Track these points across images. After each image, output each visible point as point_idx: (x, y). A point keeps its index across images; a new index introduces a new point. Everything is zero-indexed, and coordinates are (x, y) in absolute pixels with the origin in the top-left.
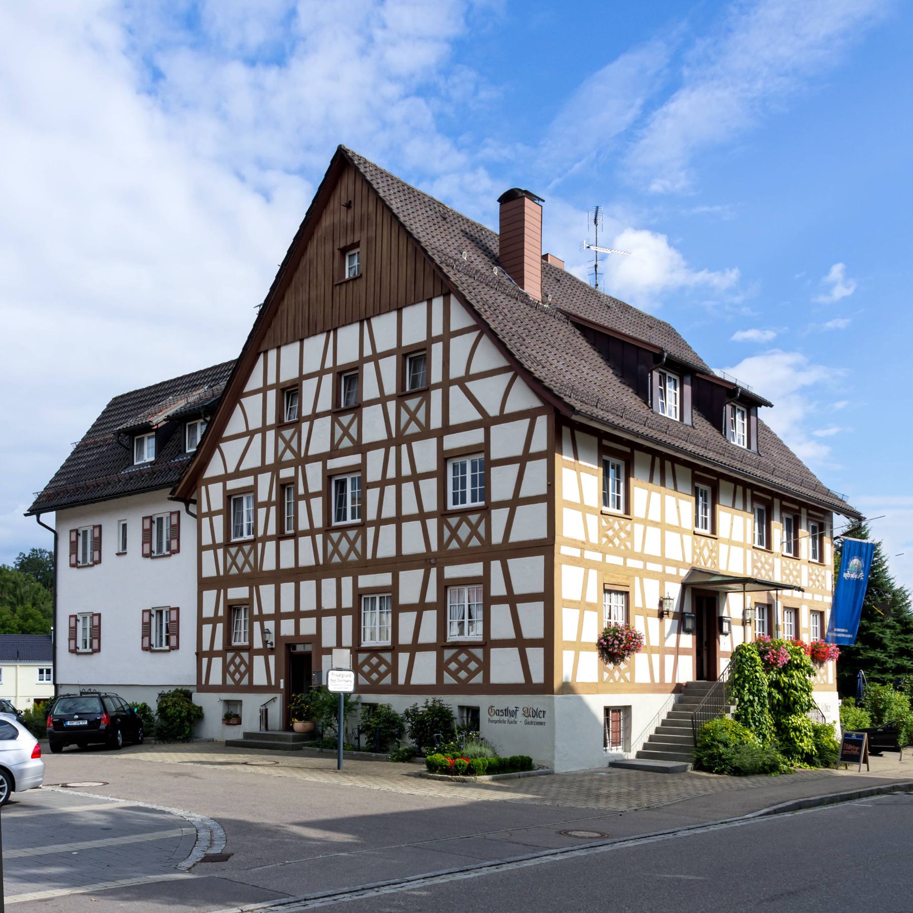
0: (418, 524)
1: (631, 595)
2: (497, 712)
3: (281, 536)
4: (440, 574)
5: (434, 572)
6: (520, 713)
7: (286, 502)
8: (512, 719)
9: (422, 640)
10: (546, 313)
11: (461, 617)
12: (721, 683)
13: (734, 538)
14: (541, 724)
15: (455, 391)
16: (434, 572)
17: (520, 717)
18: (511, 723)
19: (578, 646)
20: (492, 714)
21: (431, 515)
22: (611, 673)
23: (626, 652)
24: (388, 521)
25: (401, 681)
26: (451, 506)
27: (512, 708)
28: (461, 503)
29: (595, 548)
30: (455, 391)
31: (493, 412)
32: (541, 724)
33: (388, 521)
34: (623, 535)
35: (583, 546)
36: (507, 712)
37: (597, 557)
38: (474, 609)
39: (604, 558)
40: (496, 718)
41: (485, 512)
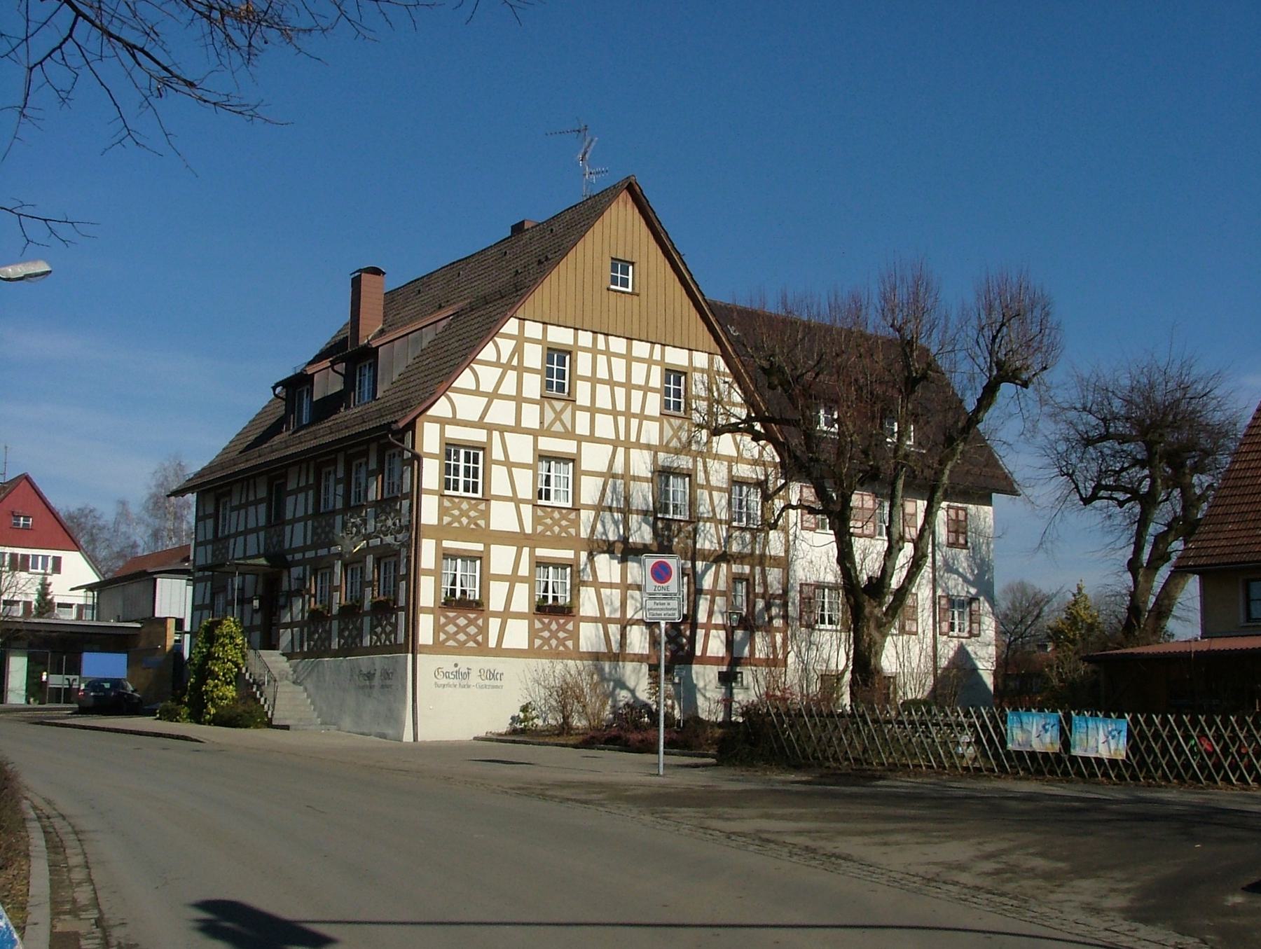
1: (487, 450)
3: (347, 507)
4: (532, 554)
5: (526, 550)
6: (474, 674)
8: (464, 682)
9: (513, 608)
11: (453, 569)
12: (470, 601)
14: (497, 687)
15: (504, 360)
16: (526, 550)
17: (474, 679)
20: (439, 677)
23: (331, 536)
25: (492, 643)
30: (504, 360)
32: (497, 687)
36: (457, 674)
40: (445, 681)
41: (576, 509)
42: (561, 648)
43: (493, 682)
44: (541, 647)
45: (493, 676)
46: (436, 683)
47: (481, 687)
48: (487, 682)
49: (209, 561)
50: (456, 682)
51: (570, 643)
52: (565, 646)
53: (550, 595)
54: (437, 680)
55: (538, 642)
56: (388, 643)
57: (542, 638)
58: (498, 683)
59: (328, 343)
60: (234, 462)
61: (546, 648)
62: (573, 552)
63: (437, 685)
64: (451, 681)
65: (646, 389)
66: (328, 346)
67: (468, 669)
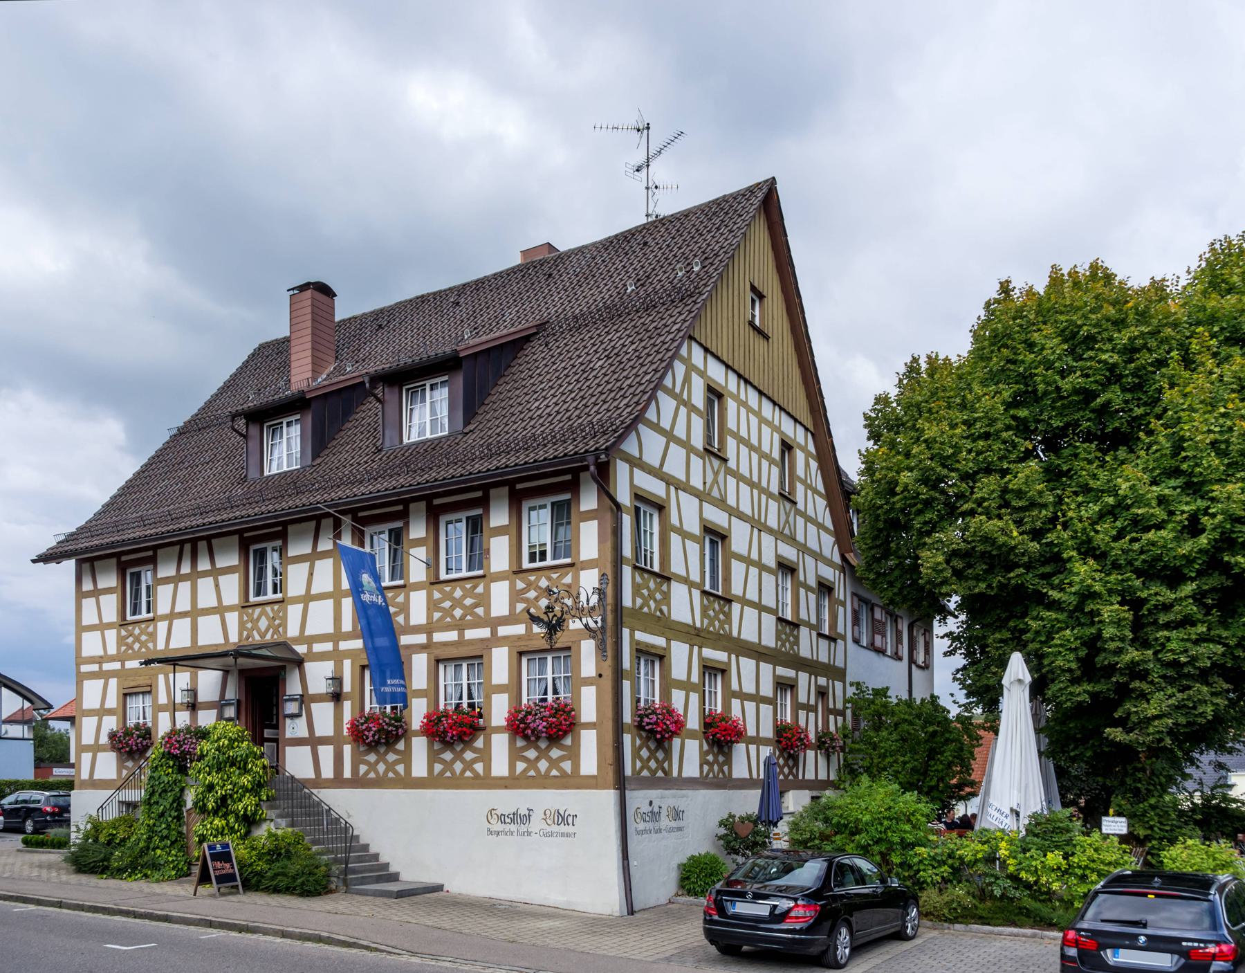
0: (216, 618)
2: (502, 818)
6: (537, 818)
7: (642, 528)
8: (523, 828)
10: (690, 296)
13: (748, 596)
17: (536, 824)
18: (523, 834)
19: (96, 748)
21: (231, 608)
22: (448, 765)
24: (183, 615)
26: (443, 576)
27: (523, 811)
28: (540, 561)
29: (112, 659)
31: (641, 427)
33: (183, 615)
34: (658, 596)
35: (100, 660)
36: (516, 818)
37: (116, 666)
38: (147, 710)
39: (100, 667)
42: (391, 775)
43: (563, 828)
44: (442, 772)
45: (563, 819)
46: (488, 830)
47: (546, 835)
48: (555, 828)
49: (234, 638)
50: (513, 827)
51: (400, 768)
52: (473, 770)
53: (465, 701)
54: (489, 826)
55: (438, 767)
56: (721, 776)
57: (526, 760)
58: (569, 829)
59: (51, 549)
60: (117, 527)
61: (448, 774)
62: (489, 629)
63: (490, 832)
64: (507, 827)
65: (172, 616)
66: (51, 552)
67: (529, 810)
